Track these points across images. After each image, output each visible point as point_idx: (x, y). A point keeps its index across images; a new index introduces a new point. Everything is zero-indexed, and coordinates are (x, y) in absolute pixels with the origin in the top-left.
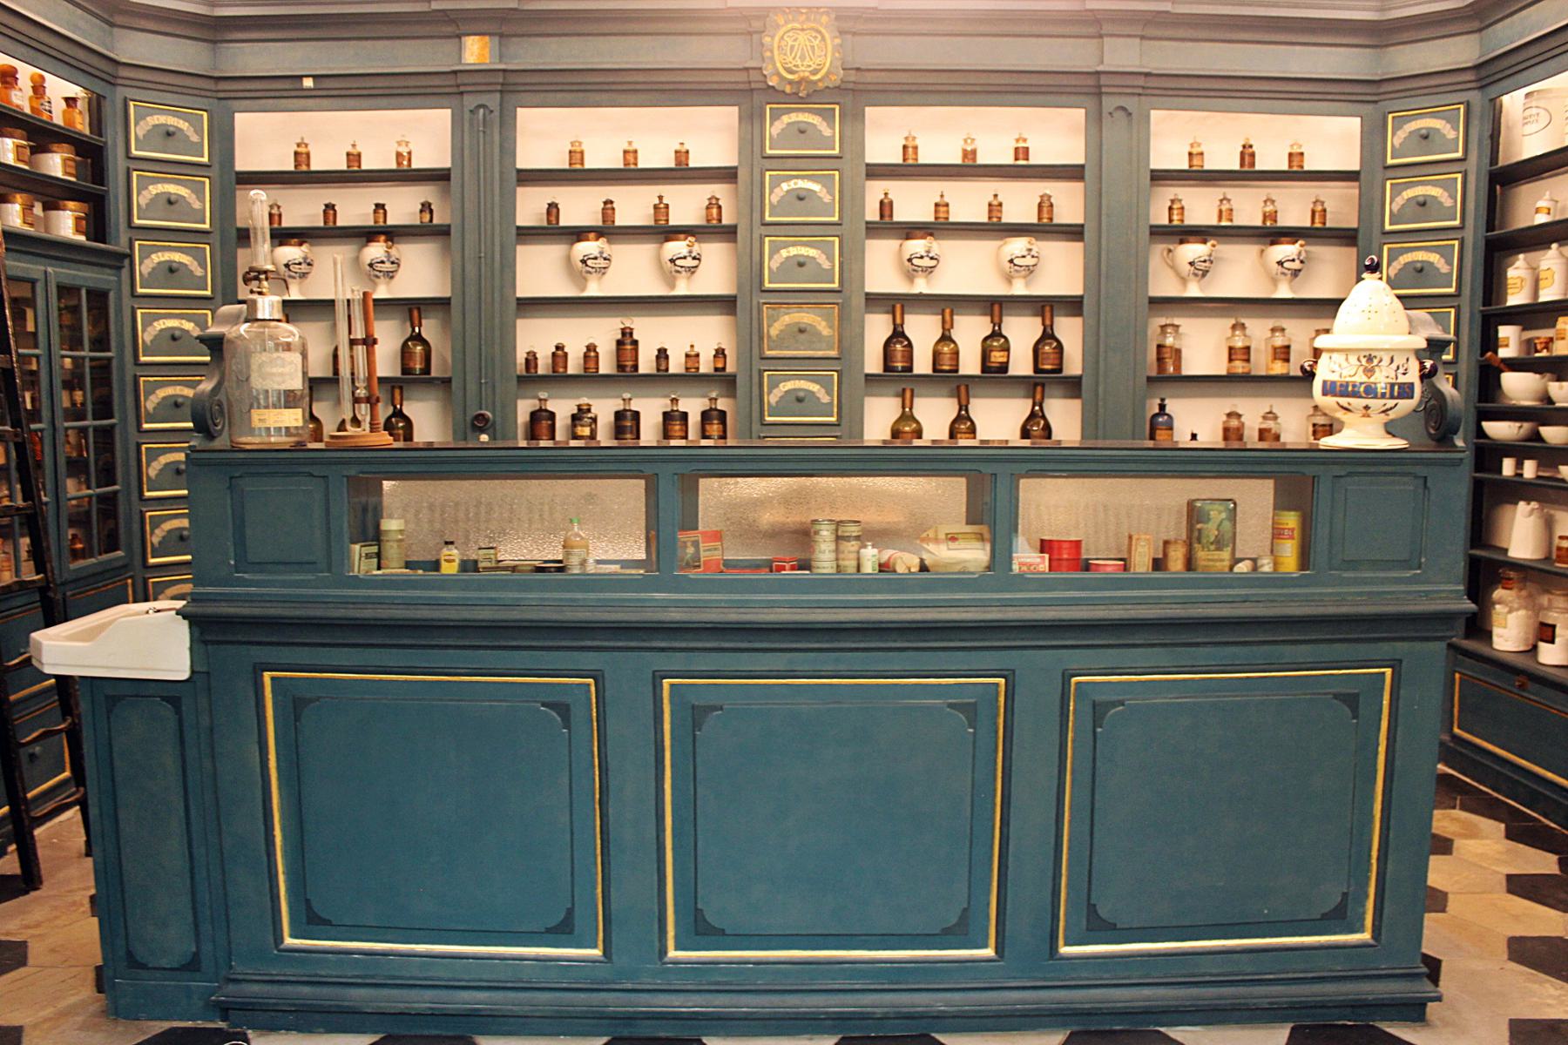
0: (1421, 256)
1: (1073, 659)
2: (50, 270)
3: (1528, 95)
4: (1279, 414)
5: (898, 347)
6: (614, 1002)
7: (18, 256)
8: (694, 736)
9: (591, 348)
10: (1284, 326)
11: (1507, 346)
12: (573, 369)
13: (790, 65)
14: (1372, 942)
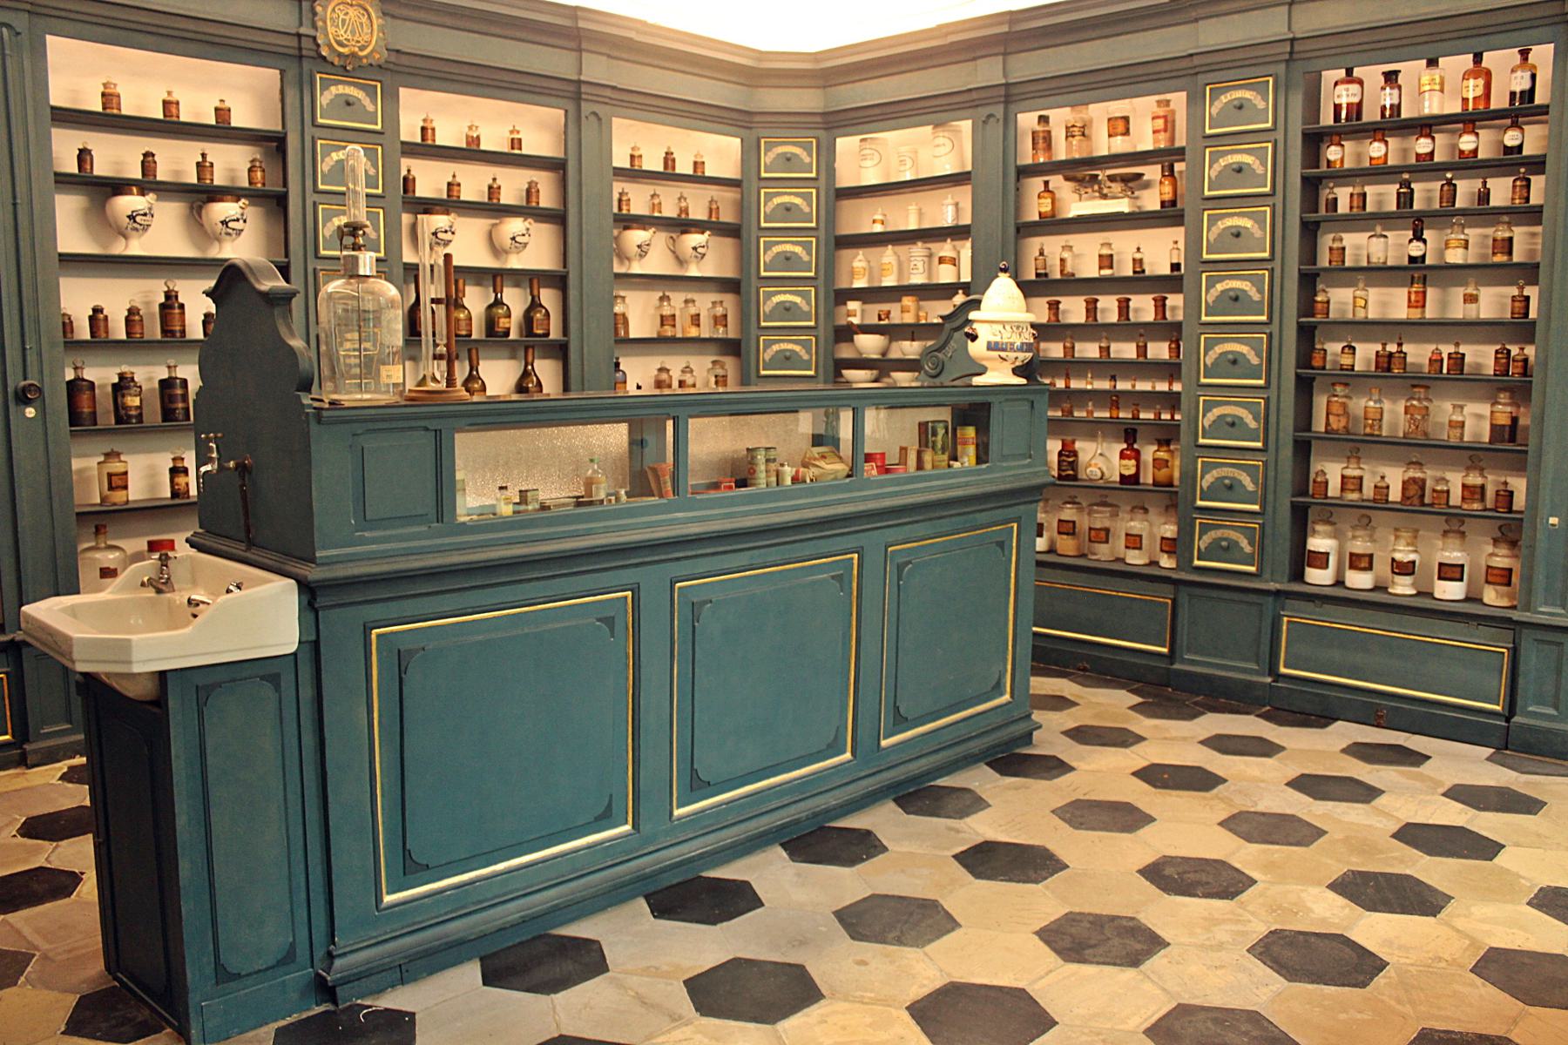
0: (789, 248)
1: (891, 534)
3: (862, 140)
8: (694, 627)
10: (695, 298)
11: (908, 312)
13: (341, 38)
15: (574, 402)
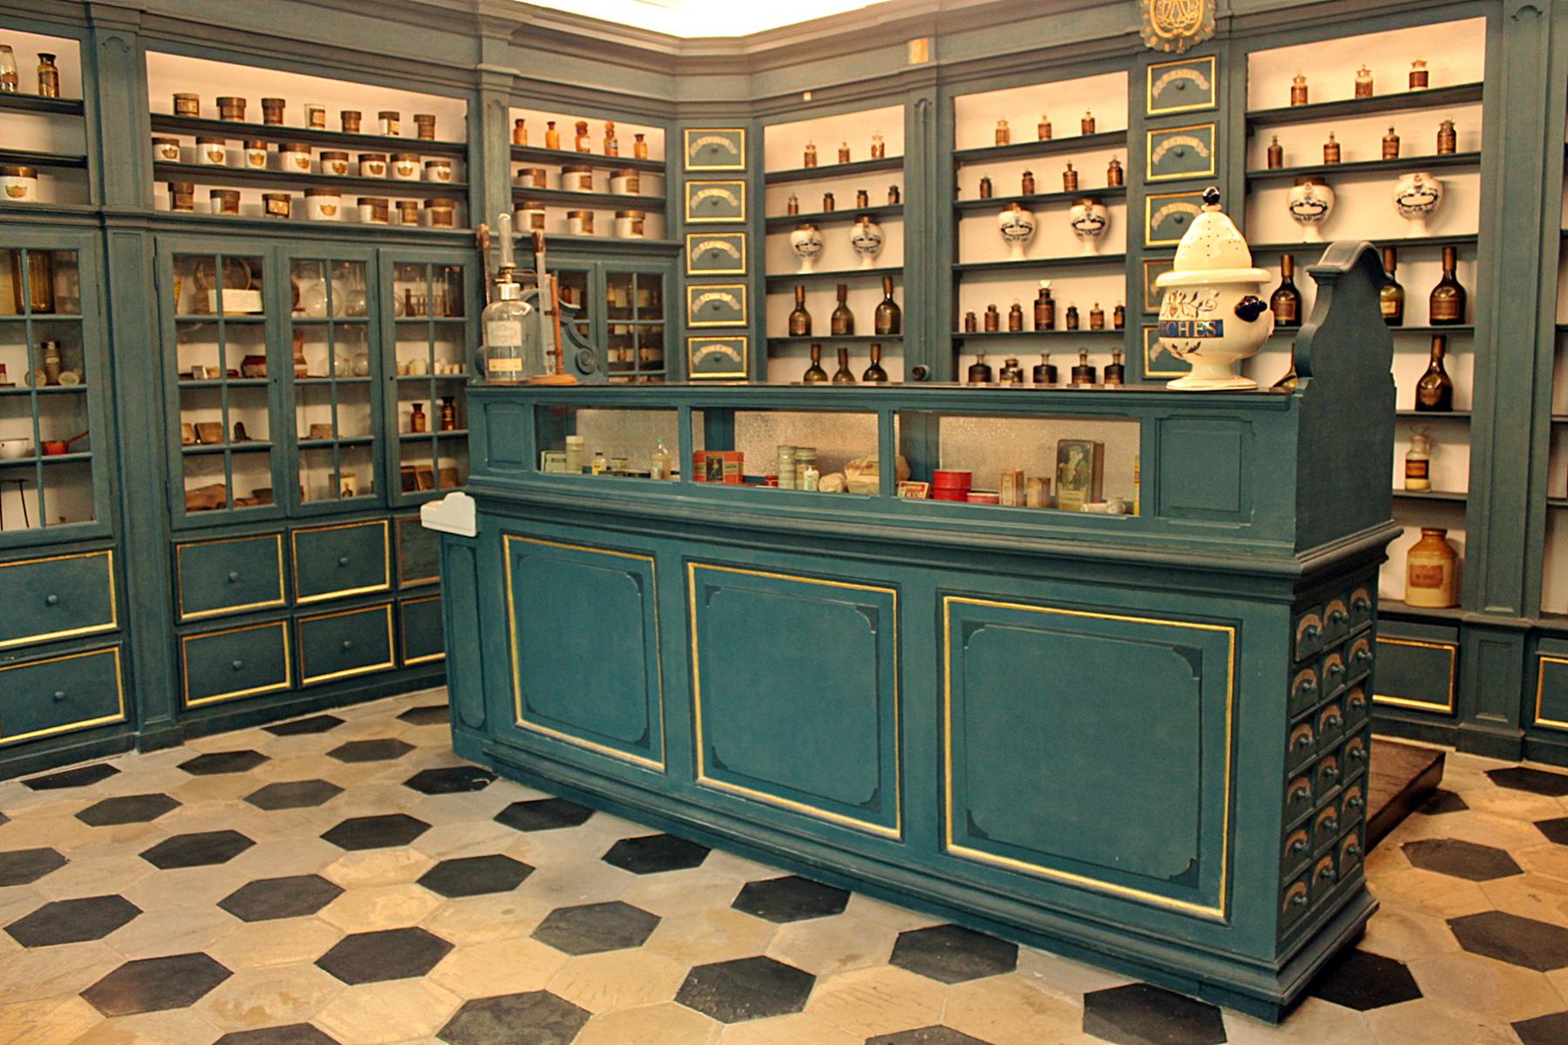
2: (599, 262)
5: (1283, 299)
6: (667, 808)
9: (1016, 308)
12: (1005, 327)
14: (1223, 921)
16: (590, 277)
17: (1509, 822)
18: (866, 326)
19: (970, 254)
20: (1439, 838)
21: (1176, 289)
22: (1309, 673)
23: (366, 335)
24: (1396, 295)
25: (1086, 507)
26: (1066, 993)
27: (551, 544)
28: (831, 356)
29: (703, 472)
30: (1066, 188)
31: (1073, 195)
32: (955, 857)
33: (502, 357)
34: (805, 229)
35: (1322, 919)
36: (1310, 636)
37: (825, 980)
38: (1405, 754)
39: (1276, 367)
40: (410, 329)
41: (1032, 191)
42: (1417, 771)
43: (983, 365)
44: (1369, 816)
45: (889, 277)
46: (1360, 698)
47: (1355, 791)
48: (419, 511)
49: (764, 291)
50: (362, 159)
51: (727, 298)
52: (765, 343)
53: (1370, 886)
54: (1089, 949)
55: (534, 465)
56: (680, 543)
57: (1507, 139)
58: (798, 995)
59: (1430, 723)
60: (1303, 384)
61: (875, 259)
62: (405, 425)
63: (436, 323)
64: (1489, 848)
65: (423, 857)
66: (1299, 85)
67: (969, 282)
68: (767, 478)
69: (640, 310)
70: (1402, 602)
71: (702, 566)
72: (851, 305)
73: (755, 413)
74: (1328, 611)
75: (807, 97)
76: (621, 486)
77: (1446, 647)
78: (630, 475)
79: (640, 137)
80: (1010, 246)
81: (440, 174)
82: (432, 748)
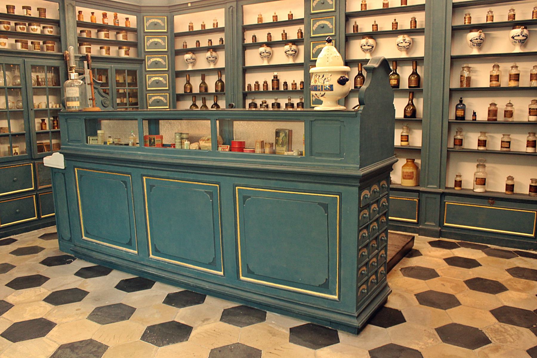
1: (237, 181)
2: (112, 66)
4: (513, 104)
6: (138, 267)
7: (107, 63)
12: (261, 89)
14: (338, 300)
15: (145, 112)
16: (109, 71)
17: (435, 259)
18: (212, 89)
19: (249, 63)
20: (412, 266)
21: (316, 74)
22: (366, 211)
23: (21, 93)
24: (397, 78)
25: (286, 153)
26: (283, 328)
27: (93, 171)
28: (200, 100)
29: (148, 143)
30: (283, 39)
31: (285, 42)
32: (243, 281)
33: (72, 101)
34: (189, 54)
35: (372, 297)
36: (366, 198)
37: (196, 329)
38: (401, 237)
39: (355, 102)
40: (39, 90)
41: (271, 40)
42: (405, 243)
43: (254, 103)
44: (388, 260)
45: (220, 71)
46: (384, 219)
47: (383, 252)
48: (43, 160)
49: (175, 77)
50: (16, 24)
51: (161, 79)
52: (175, 95)
53: (390, 284)
54: (291, 312)
55: (85, 141)
56: (140, 169)
57: (433, 24)
58: (186, 334)
59: (410, 226)
60: (362, 108)
61: (215, 65)
62: (38, 127)
63: (49, 88)
64: (429, 269)
65: (46, 291)
66: (364, 3)
67: (249, 73)
68: (171, 145)
69: (128, 83)
70: (400, 184)
71: (148, 178)
72: (207, 81)
73: (167, 121)
74: (372, 189)
75: (189, 5)
76: (118, 149)
77: (415, 200)
78: (121, 144)
79: (127, 19)
80: (263, 60)
81: (48, 31)
82: (51, 249)
